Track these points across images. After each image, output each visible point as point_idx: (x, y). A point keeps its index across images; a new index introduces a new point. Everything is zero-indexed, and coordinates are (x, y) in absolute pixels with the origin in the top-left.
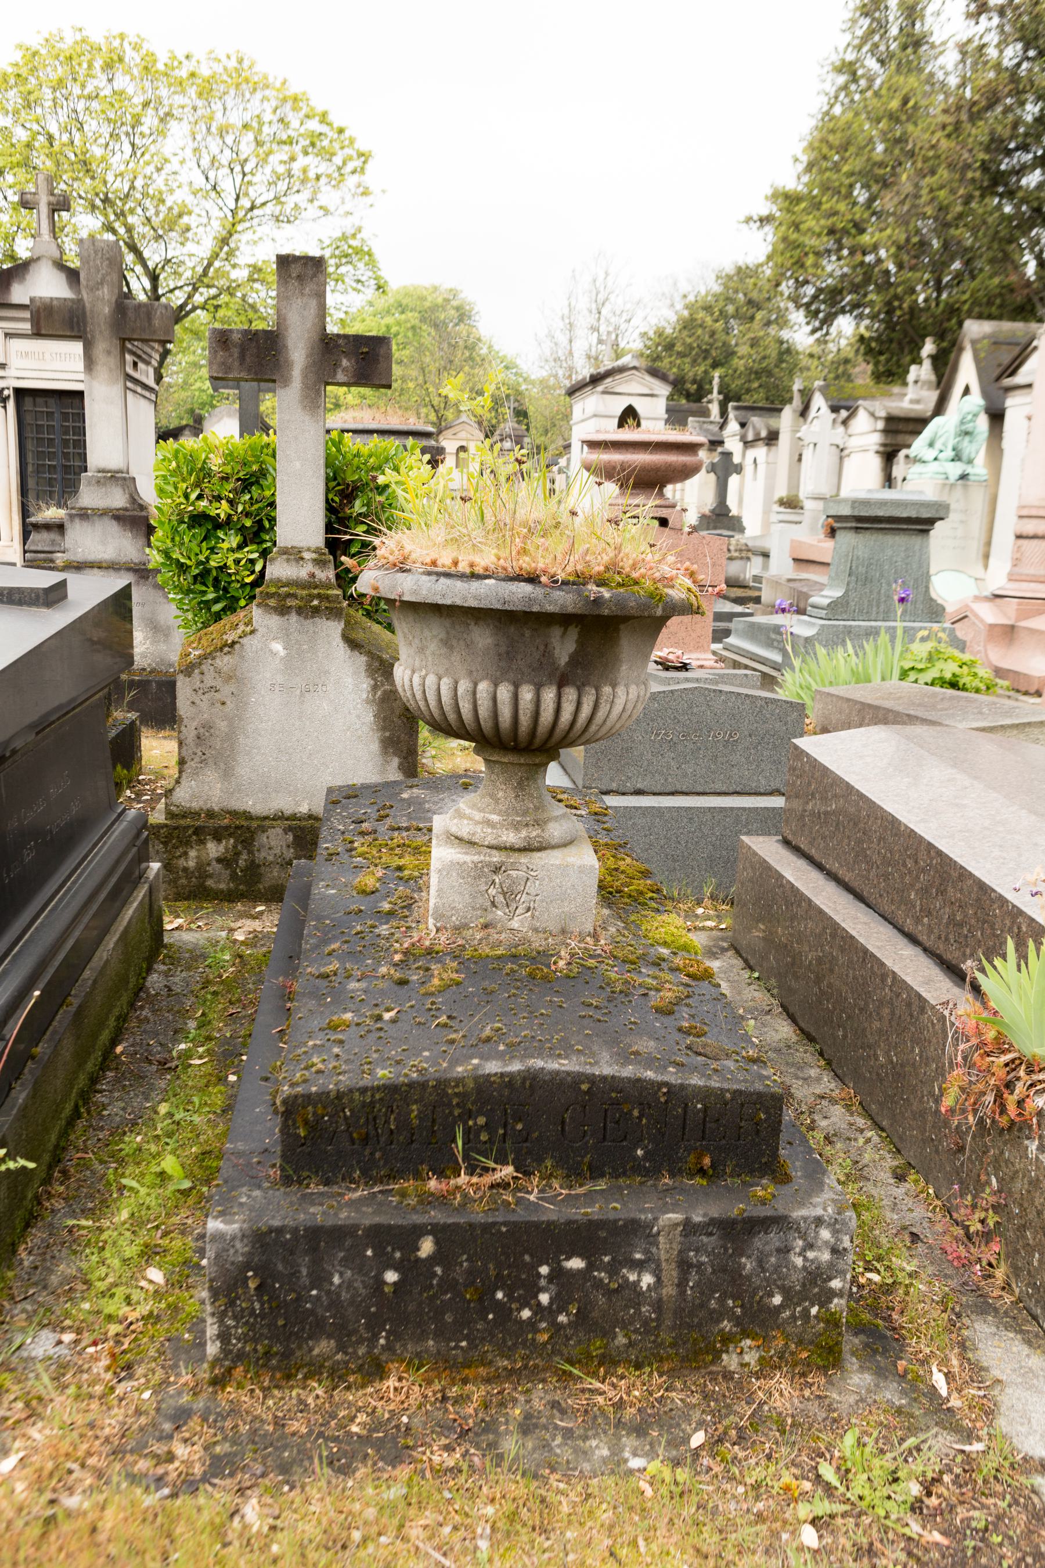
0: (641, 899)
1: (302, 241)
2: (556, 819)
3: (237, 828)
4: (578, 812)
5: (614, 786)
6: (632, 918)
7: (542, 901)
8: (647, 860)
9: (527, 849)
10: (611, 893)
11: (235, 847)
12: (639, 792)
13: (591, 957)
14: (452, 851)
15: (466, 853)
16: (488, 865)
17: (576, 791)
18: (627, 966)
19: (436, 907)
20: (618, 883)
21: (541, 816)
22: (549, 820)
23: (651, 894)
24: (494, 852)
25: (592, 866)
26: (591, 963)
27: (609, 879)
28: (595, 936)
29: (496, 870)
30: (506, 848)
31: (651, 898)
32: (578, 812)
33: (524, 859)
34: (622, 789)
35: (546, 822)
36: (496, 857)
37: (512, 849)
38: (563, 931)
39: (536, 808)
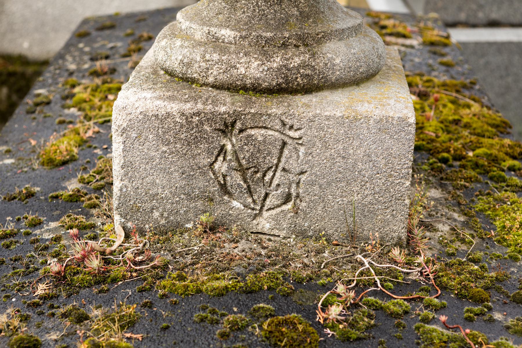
0: (495, 172)
1: (472, 80)
2: (341, 35)
3: (11, 74)
4: (408, 42)
5: (462, 17)
6: (479, 205)
7: (312, 183)
8: (504, 108)
9: (285, 88)
10: (445, 161)
11: (9, 97)
12: (493, 24)
13: (400, 288)
14: (148, 94)
15: (171, 99)
16: (211, 118)
17: (411, 17)
18: (469, 308)
19: (123, 195)
20: (457, 145)
21: (311, 28)
22: (326, 37)
23: (510, 162)
24: (225, 96)
25: (403, 120)
26: (397, 303)
27: (444, 137)
28: (409, 244)
29: (227, 128)
30: (245, 89)
31: (511, 169)
32: (408, 42)
33: (275, 107)
34: (472, 21)
35: (321, 39)
36: (226, 105)
37: (256, 89)
38: (353, 237)
39: (304, 16)
